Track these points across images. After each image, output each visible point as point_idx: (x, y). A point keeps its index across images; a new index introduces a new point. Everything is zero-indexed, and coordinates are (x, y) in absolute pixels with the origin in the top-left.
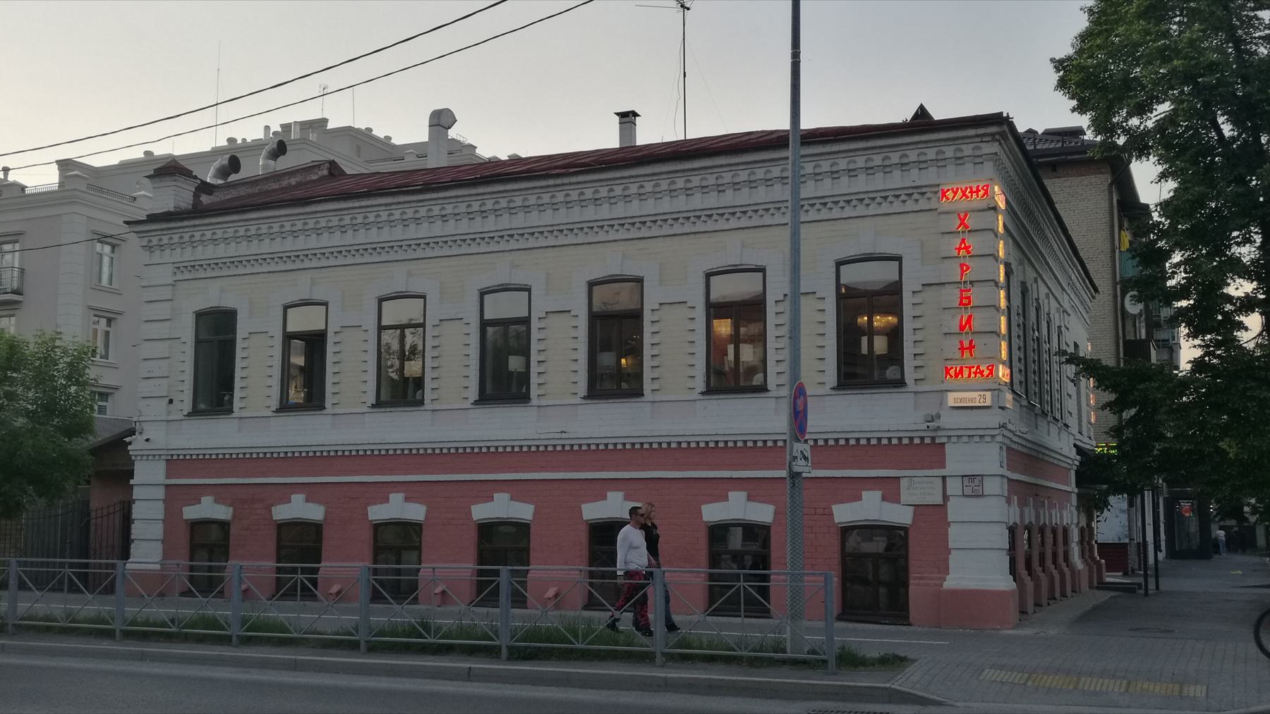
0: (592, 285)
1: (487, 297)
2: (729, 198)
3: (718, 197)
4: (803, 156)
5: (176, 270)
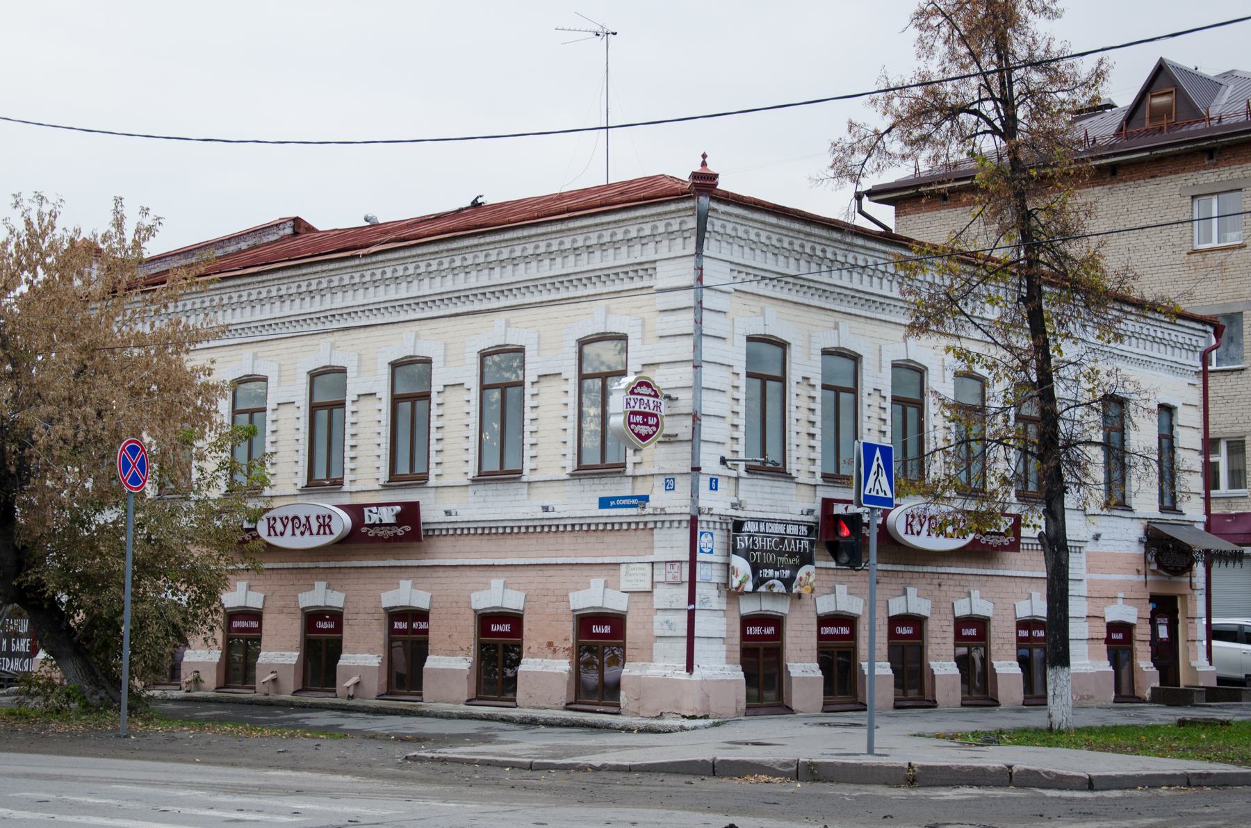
0: (484, 355)
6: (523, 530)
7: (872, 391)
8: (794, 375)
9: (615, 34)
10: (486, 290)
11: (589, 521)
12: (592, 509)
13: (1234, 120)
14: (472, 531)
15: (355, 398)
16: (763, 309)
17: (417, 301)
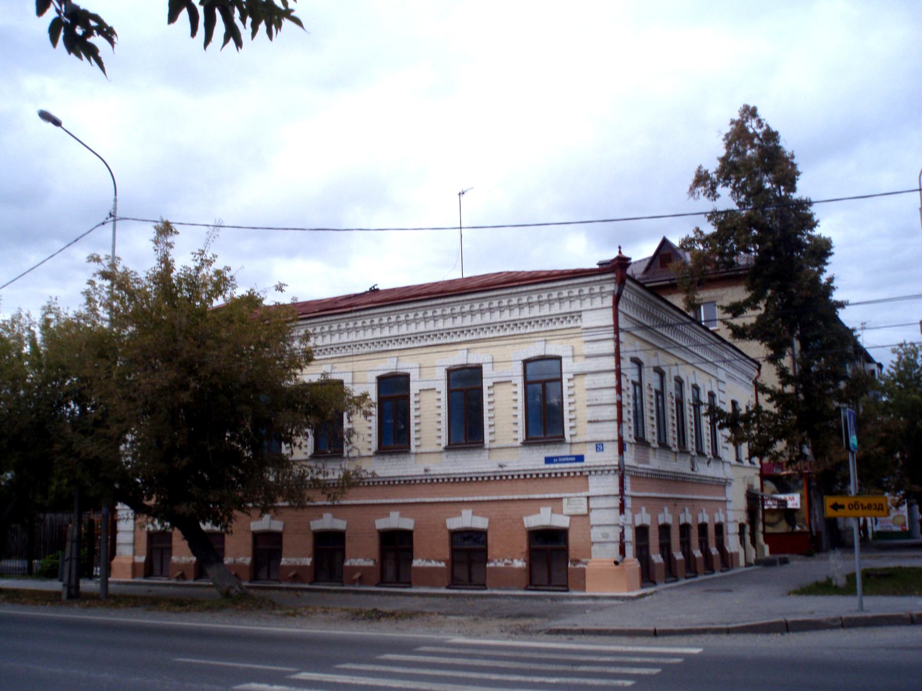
1: (529, 366)
2: (459, 322)
12: (542, 465)
15: (571, 376)
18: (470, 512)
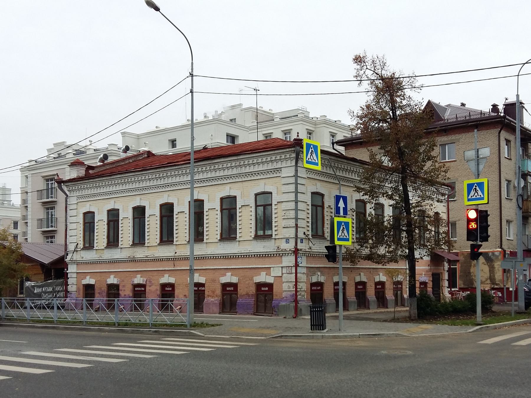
1: (258, 197)
3: (286, 163)
4: (194, 166)
5: (77, 198)
6: (237, 257)
7: (350, 210)
8: (326, 205)
9: (259, 90)
10: (223, 177)
11: (260, 254)
13: (452, 121)
14: (219, 257)
16: (316, 184)
17: (198, 181)
18: (167, 275)
